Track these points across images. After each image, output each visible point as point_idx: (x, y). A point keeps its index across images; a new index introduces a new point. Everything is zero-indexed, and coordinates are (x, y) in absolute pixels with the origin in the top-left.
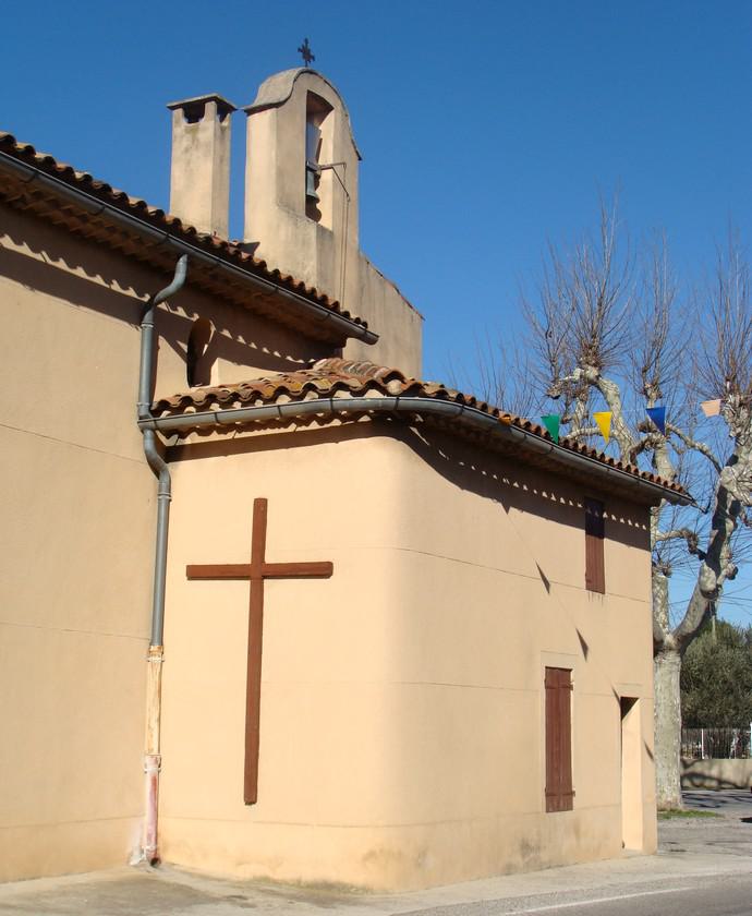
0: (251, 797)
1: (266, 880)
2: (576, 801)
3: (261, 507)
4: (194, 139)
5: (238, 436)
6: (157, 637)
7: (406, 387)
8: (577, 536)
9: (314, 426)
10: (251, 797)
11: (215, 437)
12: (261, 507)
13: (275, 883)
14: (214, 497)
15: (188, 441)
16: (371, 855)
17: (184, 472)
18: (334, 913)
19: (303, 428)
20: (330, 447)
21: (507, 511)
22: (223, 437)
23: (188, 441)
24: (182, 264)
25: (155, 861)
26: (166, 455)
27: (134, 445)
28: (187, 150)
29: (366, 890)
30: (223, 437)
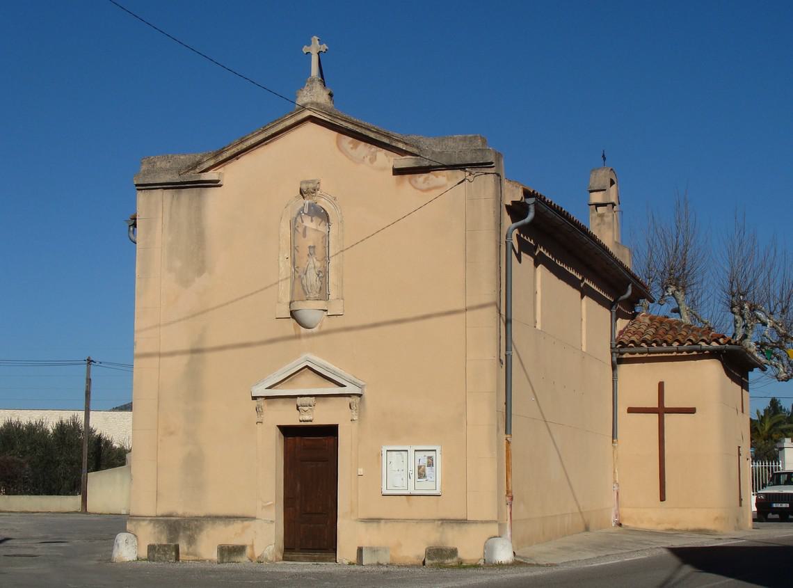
0: (663, 498)
1: (672, 530)
2: (357, 549)
3: (661, 385)
4: (602, 220)
5: (649, 356)
6: (614, 436)
7: (726, 341)
8: (740, 387)
9: (685, 354)
10: (663, 498)
11: (637, 355)
12: (661, 385)
13: (676, 530)
14: (640, 381)
15: (624, 356)
16: (716, 519)
17: (623, 368)
18: (463, 583)
19: (680, 354)
20: (692, 362)
21: (744, 386)
22: (641, 356)
23: (624, 356)
24: (630, 287)
25: (620, 525)
26: (618, 361)
27: (607, 358)
28: (598, 225)
29: (715, 531)
30: (641, 356)
